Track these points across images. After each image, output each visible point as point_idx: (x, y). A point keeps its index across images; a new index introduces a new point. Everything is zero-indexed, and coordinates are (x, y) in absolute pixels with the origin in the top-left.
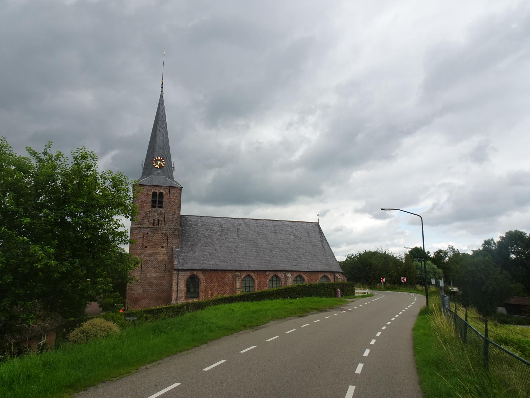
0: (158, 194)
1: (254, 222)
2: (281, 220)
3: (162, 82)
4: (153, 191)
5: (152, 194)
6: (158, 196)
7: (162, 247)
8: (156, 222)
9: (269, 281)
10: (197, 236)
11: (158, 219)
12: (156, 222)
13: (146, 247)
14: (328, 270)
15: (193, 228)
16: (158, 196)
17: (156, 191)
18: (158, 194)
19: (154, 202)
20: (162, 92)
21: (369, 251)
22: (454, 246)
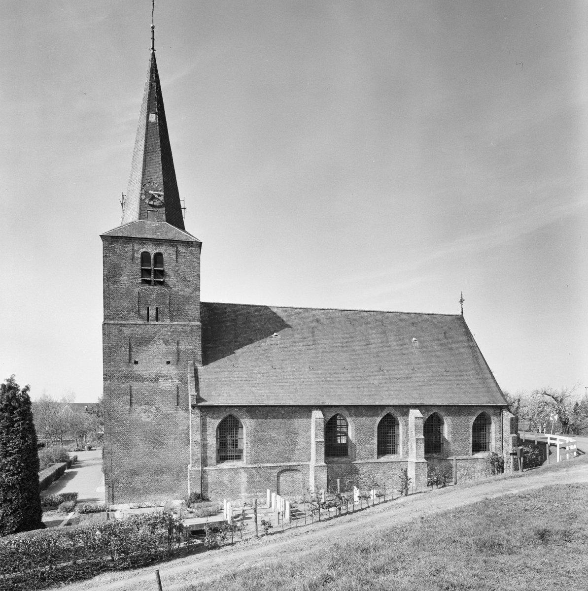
0: (152, 256)
1: (344, 314)
2: (400, 311)
3: (153, 28)
4: (142, 250)
5: (140, 256)
6: (152, 261)
7: (168, 363)
8: (152, 313)
9: (278, 493)
10: (236, 342)
11: (157, 308)
12: (152, 313)
13: (136, 363)
14: (489, 402)
15: (228, 327)
16: (152, 261)
17: (149, 250)
18: (152, 256)
19: (145, 272)
20: (153, 49)
21: (22, 387)
22: (31, 390)
